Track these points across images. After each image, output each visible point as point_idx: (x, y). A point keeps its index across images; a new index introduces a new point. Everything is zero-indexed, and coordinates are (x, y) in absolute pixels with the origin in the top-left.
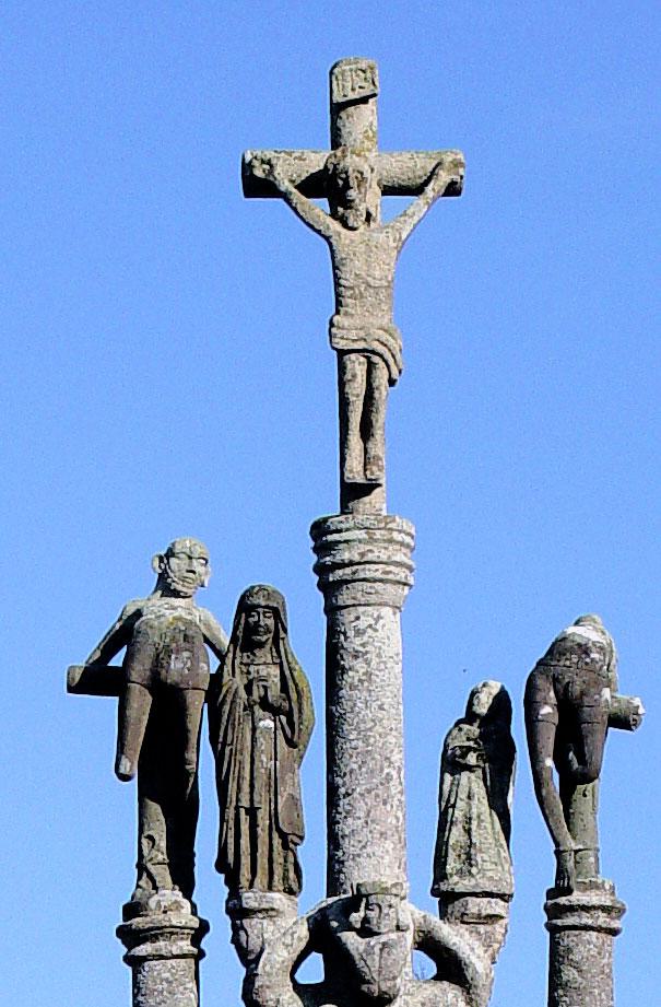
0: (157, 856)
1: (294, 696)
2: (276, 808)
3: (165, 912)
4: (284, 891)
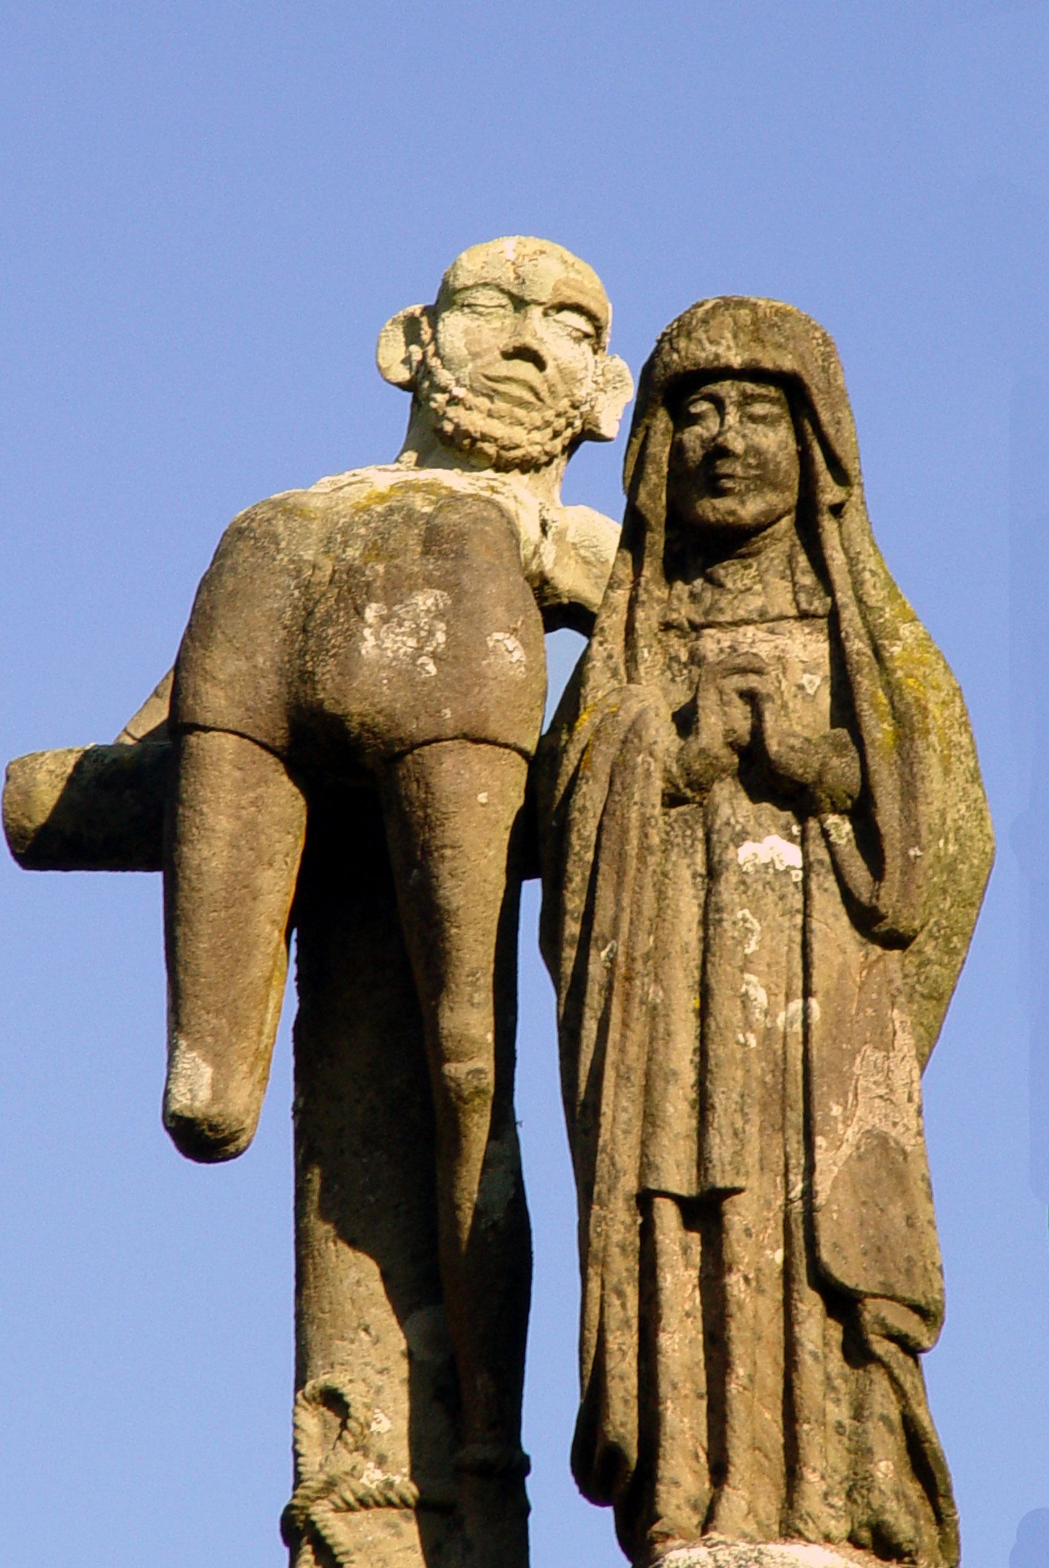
0: (353, 1472)
1: (879, 730)
2: (809, 1194)
4: (854, 1540)
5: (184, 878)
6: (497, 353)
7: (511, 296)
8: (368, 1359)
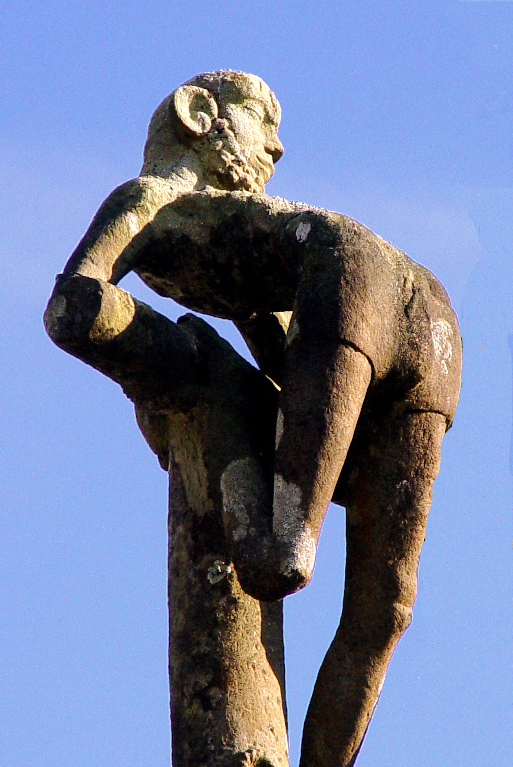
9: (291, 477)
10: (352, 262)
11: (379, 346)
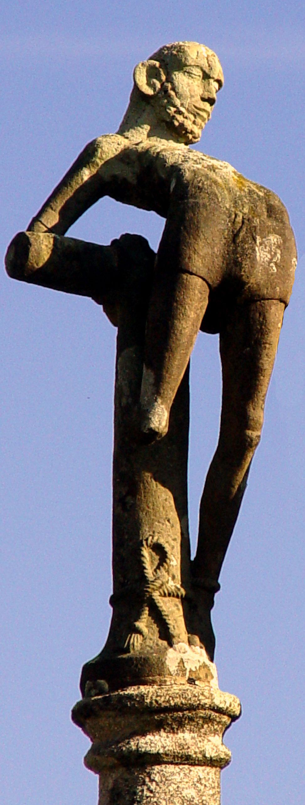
3: (191, 681)
5: (174, 333)
6: (199, 97)
7: (204, 72)
8: (169, 533)
9: (150, 366)
10: (190, 211)
11: (210, 267)
